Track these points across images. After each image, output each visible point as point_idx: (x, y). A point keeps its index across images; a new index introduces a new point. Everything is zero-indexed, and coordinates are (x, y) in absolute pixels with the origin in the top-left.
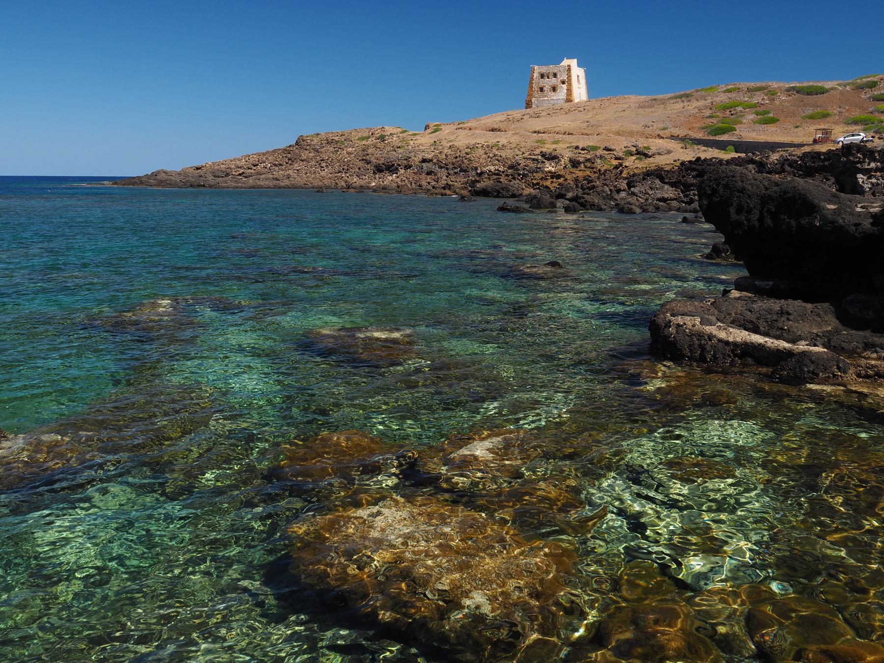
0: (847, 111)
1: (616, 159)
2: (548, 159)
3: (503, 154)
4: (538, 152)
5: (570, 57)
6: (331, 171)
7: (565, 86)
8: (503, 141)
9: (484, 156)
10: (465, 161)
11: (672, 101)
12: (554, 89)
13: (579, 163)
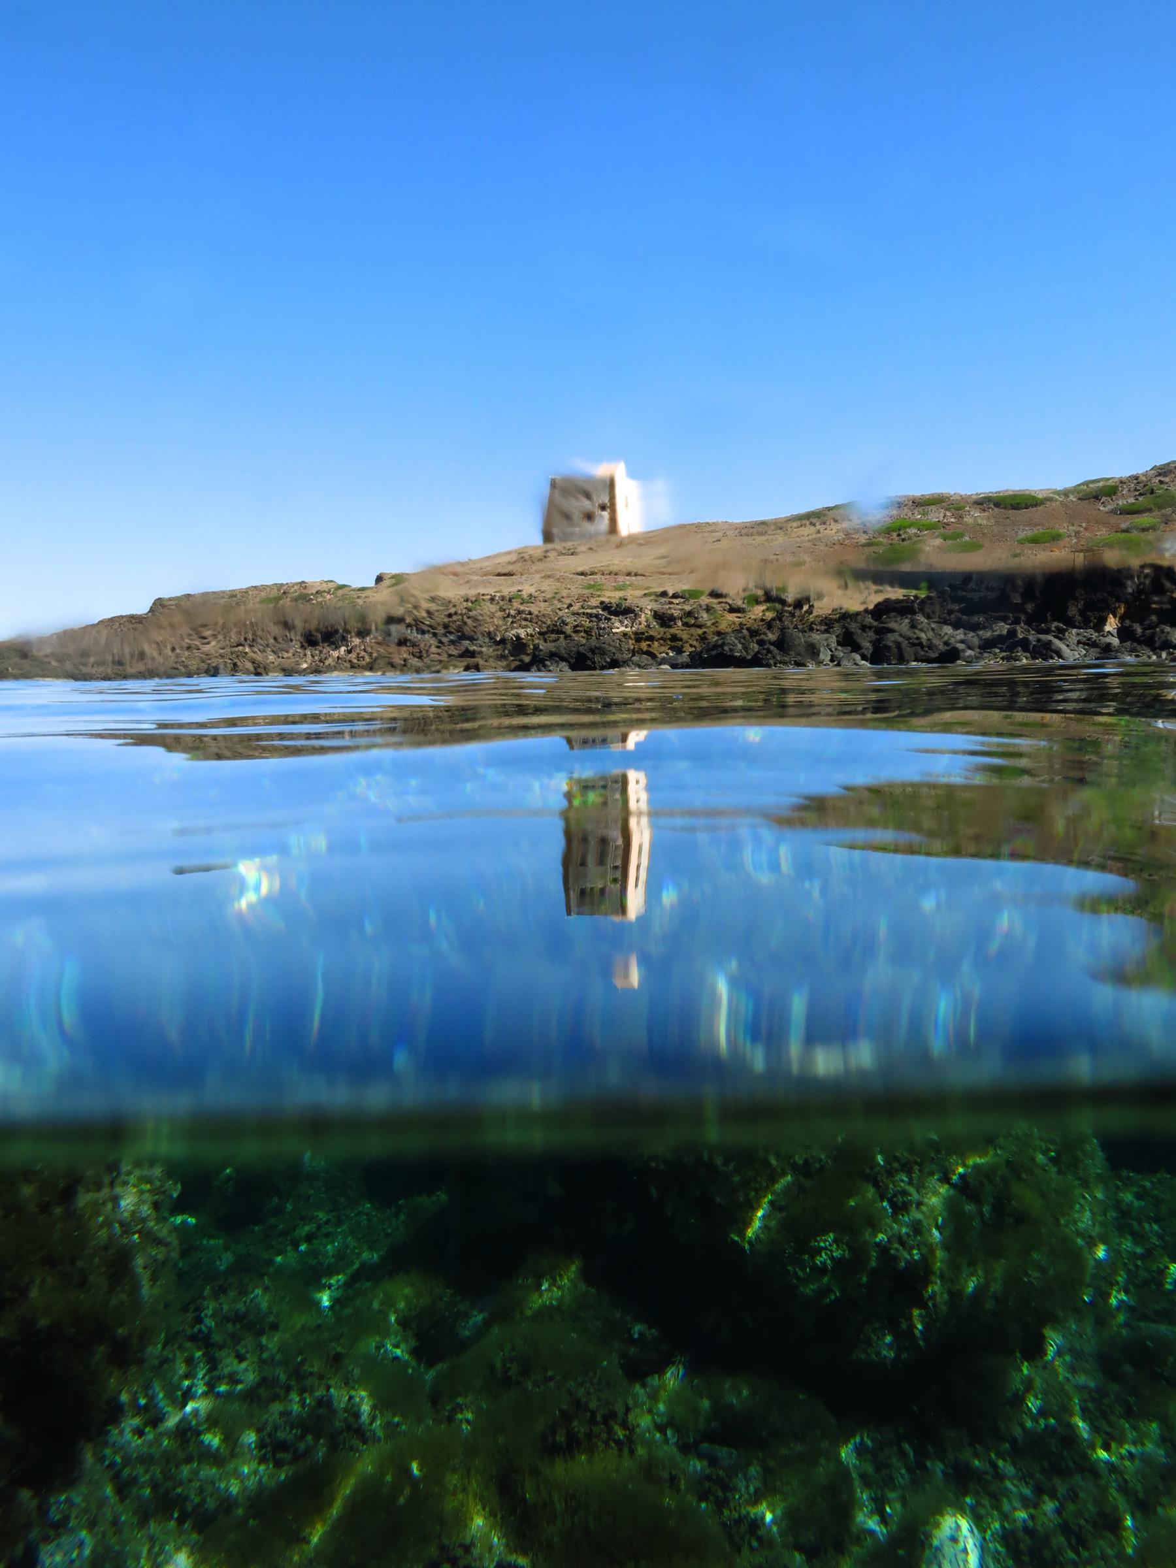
0: (1086, 529)
1: (732, 610)
2: (616, 613)
3: (534, 609)
4: (594, 602)
5: (613, 457)
6: (223, 644)
7: (606, 514)
8: (528, 589)
9: (500, 614)
10: (469, 622)
11: (795, 524)
12: (589, 517)
13: (672, 618)
